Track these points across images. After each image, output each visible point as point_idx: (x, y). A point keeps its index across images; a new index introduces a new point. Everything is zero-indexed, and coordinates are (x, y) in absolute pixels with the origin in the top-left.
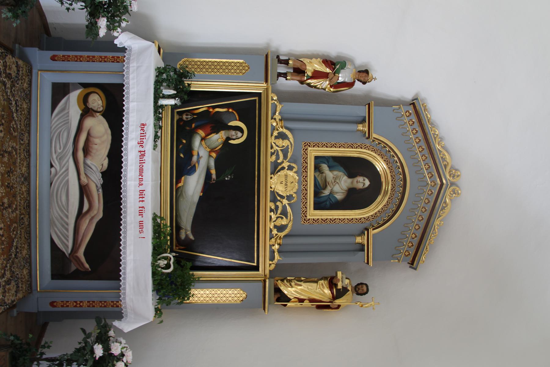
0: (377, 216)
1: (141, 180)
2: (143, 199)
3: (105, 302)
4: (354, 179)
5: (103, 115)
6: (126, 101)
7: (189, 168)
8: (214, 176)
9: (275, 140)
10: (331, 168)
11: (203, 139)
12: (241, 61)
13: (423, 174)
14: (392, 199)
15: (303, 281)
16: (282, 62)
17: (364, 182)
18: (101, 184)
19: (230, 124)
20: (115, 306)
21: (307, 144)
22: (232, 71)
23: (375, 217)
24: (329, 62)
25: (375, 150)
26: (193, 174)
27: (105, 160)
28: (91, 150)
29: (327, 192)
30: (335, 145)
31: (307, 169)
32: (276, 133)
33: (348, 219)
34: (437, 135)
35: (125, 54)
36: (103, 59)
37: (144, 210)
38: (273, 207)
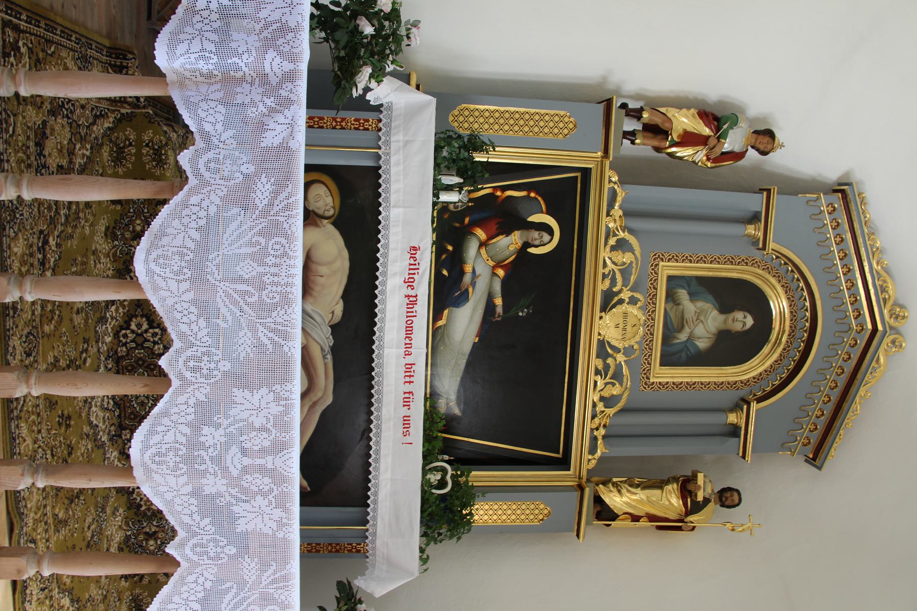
0: (762, 378)
1: (408, 346)
2: (412, 379)
3: (337, 544)
4: (729, 315)
5: (335, 224)
6: (384, 205)
7: (456, 294)
8: (499, 310)
9: (611, 252)
10: (693, 296)
11: (482, 244)
12: (562, 113)
13: (845, 312)
14: (788, 350)
15: (642, 486)
16: (631, 113)
17: (745, 320)
18: (330, 346)
19: (530, 219)
20: (354, 550)
21: (659, 255)
22: (546, 130)
23: (758, 379)
24: (711, 117)
25: (768, 268)
26: (464, 304)
27: (337, 304)
28: (312, 285)
29: (683, 337)
30: (704, 259)
31: (656, 299)
32: (612, 241)
33: (715, 383)
34: (878, 249)
35: (381, 116)
36: (339, 124)
37: (412, 397)
38: (600, 367)
